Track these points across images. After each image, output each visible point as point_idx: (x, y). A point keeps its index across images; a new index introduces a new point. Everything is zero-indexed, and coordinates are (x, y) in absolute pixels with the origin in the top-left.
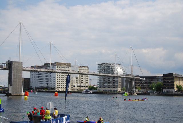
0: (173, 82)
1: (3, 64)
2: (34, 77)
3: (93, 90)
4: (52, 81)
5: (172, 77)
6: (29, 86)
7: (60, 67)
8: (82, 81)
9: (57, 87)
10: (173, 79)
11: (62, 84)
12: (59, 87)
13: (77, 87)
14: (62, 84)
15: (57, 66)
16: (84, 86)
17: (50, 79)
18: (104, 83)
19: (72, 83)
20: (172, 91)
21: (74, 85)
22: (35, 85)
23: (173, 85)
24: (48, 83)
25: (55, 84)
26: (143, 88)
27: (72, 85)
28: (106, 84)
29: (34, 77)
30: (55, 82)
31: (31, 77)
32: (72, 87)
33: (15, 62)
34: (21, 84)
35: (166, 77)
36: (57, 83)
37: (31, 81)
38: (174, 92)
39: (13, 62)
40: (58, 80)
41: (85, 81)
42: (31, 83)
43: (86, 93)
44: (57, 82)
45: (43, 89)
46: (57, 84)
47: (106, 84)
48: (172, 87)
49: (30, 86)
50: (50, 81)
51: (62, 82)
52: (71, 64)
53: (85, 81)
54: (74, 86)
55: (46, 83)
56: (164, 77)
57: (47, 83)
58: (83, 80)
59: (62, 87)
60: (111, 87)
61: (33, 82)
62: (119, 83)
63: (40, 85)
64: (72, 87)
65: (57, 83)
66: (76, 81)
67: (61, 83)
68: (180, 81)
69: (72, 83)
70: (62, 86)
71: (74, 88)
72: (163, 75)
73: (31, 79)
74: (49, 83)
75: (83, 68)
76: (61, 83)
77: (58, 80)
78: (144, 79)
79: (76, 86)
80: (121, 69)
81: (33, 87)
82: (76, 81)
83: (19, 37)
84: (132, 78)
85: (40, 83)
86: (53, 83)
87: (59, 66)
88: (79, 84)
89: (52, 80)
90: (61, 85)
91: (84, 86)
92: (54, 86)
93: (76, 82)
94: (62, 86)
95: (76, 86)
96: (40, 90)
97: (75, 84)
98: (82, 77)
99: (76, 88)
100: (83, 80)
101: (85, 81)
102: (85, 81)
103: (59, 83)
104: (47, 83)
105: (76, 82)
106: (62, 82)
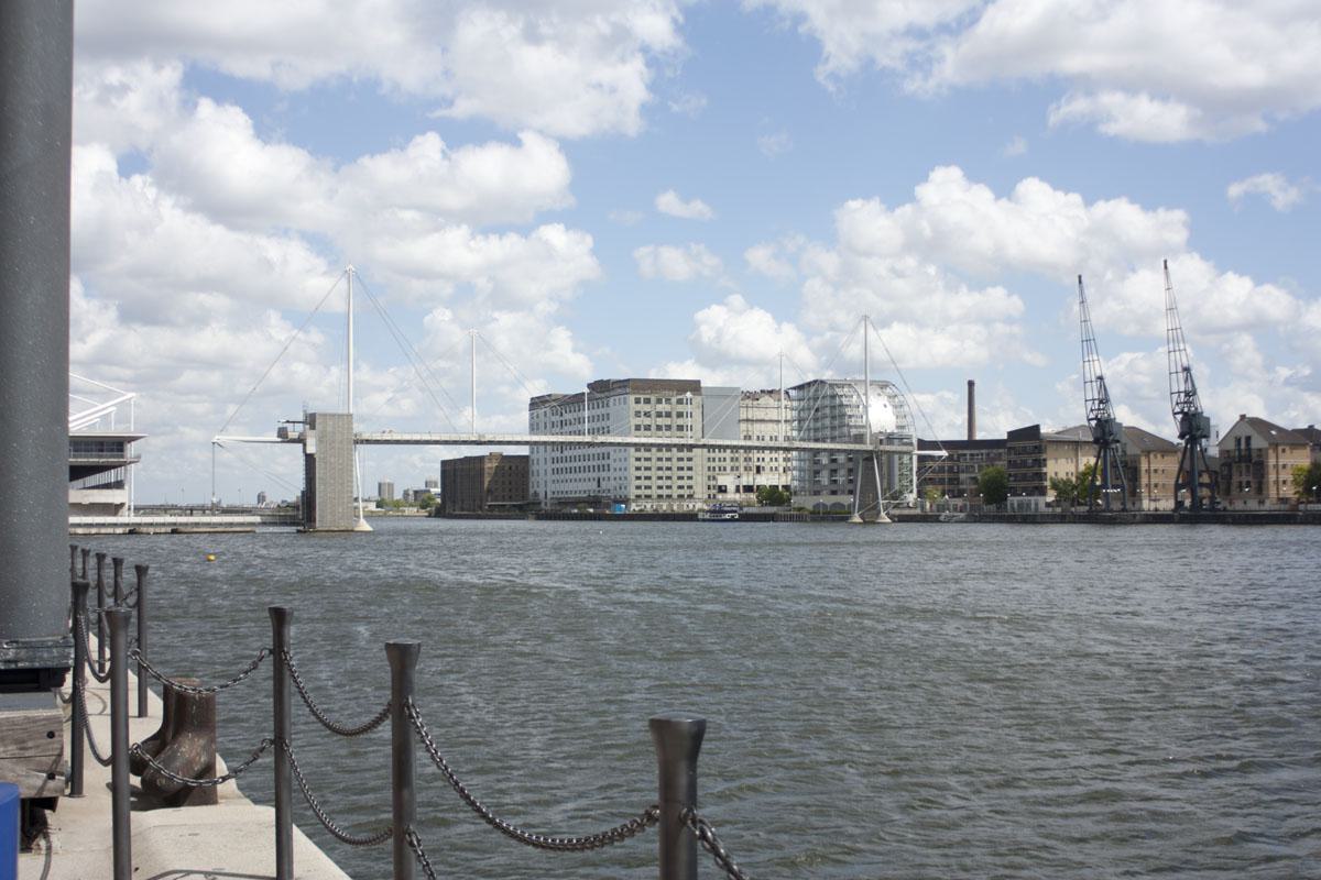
0: (1042, 463)
1: (288, 422)
3: (774, 501)
5: (1037, 443)
6: (528, 491)
7: (647, 401)
8: (761, 464)
9: (639, 492)
10: (1039, 449)
11: (660, 478)
12: (648, 492)
13: (738, 490)
14: (660, 478)
15: (632, 398)
18: (817, 473)
19: (711, 473)
20: (1036, 504)
21: (722, 480)
22: (551, 488)
23: (1041, 476)
24: (603, 474)
25: (626, 478)
26: (960, 494)
27: (712, 483)
30: (625, 469)
32: (713, 492)
33: (325, 415)
35: (1021, 444)
36: (639, 473)
37: (534, 468)
38: (1042, 508)
39: (317, 417)
40: (644, 464)
41: (776, 464)
42: (532, 479)
43: (713, 521)
44: (638, 469)
45: (576, 502)
46: (638, 478)
47: (824, 479)
48: (1036, 488)
49: (531, 491)
51: (660, 469)
52: (702, 385)
53: (776, 464)
54: (722, 489)
55: (592, 475)
57: (595, 475)
59: (660, 492)
61: (542, 472)
63: (570, 487)
64: (713, 492)
65: (639, 473)
66: (728, 464)
67: (653, 473)
68: (1077, 456)
69: (711, 473)
70: (660, 487)
71: (720, 496)
73: (534, 457)
75: (765, 400)
76: (653, 473)
77: (644, 464)
78: (944, 453)
79: (731, 488)
80: (890, 408)
81: (542, 496)
82: (728, 464)
83: (346, 333)
84: (871, 452)
85: (562, 477)
86: (618, 474)
87: (642, 397)
88: (746, 480)
90: (654, 483)
92: (622, 493)
93: (728, 469)
94: (660, 487)
95: (731, 488)
96: (564, 510)
97: (727, 480)
99: (731, 496)
101: (774, 464)
102: (774, 464)
103: (648, 473)
104: (595, 475)
105: (728, 469)
106: (660, 469)
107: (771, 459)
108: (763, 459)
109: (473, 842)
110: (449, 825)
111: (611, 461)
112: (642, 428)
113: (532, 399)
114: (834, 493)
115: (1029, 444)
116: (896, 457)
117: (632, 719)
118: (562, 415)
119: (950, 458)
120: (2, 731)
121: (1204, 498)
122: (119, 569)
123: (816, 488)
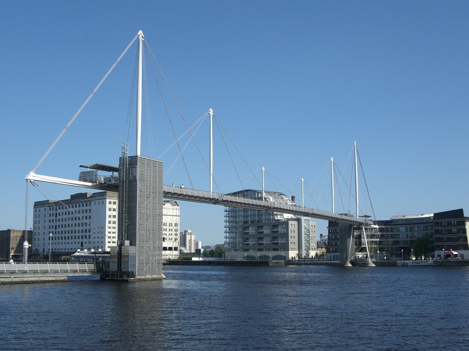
2: (44, 227)
4: (96, 235)
16: (170, 249)
17: (90, 232)
18: (261, 239)
24: (84, 240)
25: (102, 242)
28: (251, 242)
29: (44, 227)
31: (35, 228)
34: (254, 260)
50: (89, 236)
56: (436, 221)
57: (80, 240)
58: (168, 234)
60: (269, 250)
61: (41, 240)
62: (290, 239)
63: (61, 246)
72: (432, 215)
73: (37, 231)
74: (87, 240)
81: (41, 251)
86: (96, 240)
89: (94, 233)
91: (170, 249)
98: (171, 228)
100: (168, 234)
102: (171, 237)
104: (80, 240)
107: (170, 234)
108: (166, 234)
109: (168, 342)
110: (297, 219)
111: (91, 234)
112: (112, 217)
113: (35, 203)
114: (275, 250)
115: (454, 221)
116: (446, 225)
117: (198, 325)
118: (56, 210)
119: (380, 230)
120: (1, 304)
121: (444, 250)
122: (120, 252)
123: (246, 247)
